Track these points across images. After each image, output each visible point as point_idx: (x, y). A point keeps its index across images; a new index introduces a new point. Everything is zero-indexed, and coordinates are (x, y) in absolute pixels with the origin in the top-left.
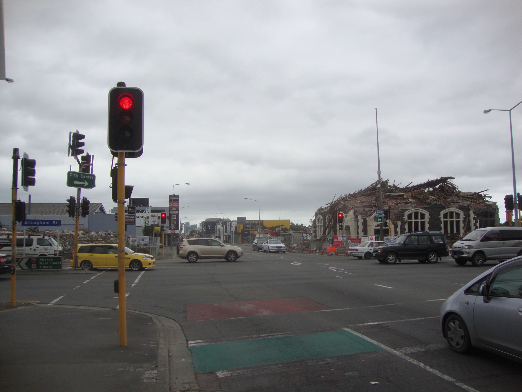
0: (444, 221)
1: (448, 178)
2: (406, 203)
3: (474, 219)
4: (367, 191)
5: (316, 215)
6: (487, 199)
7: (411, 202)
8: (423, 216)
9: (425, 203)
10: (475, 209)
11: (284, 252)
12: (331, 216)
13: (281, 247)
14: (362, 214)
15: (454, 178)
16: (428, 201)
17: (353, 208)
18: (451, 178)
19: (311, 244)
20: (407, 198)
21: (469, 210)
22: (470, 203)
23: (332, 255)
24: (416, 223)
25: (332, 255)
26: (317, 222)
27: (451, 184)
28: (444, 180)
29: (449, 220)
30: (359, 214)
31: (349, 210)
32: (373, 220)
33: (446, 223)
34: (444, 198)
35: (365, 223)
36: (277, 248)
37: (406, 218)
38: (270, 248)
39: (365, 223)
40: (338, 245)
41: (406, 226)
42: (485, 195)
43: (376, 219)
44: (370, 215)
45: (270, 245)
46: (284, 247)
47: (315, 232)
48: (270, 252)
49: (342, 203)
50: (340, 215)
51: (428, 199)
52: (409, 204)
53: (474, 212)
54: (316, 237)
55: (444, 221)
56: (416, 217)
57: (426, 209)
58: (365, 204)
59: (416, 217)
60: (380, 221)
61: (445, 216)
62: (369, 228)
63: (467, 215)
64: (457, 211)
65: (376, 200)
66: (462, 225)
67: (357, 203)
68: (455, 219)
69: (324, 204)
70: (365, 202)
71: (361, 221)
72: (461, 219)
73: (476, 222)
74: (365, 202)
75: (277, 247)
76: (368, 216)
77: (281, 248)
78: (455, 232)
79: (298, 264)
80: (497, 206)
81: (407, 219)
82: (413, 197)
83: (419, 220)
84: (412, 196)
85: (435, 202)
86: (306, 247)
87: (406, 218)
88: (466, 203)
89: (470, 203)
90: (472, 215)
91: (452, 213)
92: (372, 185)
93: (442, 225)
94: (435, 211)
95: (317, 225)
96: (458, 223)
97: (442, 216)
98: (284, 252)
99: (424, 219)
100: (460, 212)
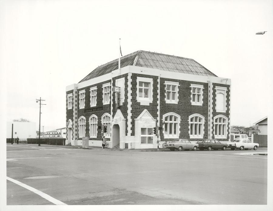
56: (171, 120)
61: (192, 120)
93: (189, 127)
97: (189, 120)
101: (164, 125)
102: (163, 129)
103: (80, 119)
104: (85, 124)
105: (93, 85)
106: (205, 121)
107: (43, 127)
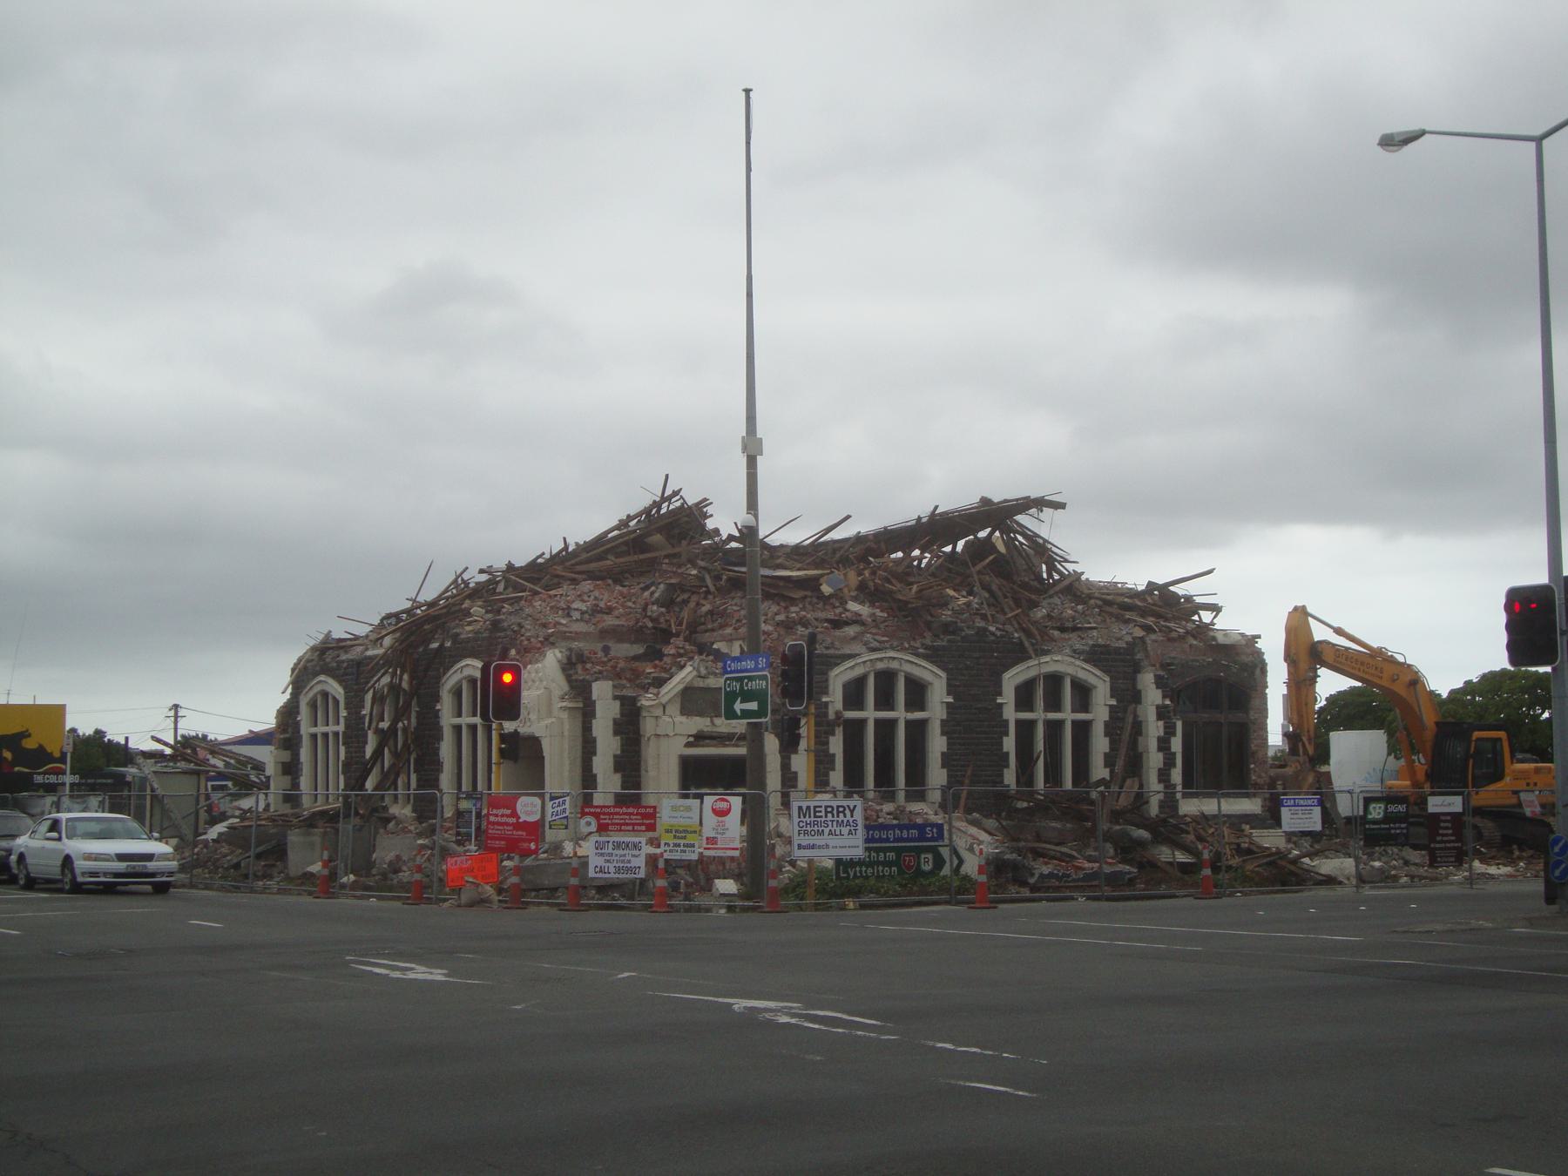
0: (1019, 723)
1: (1026, 505)
2: (837, 624)
3: (1162, 713)
4: (600, 558)
5: (302, 676)
6: (1206, 616)
7: (857, 620)
8: (917, 693)
9: (928, 625)
10: (1164, 666)
11: (161, 889)
12: (411, 682)
13: (149, 857)
14: (616, 675)
15: (1062, 506)
16: (946, 615)
17: (548, 642)
18: (1040, 503)
19: (294, 838)
20: (839, 598)
21: (1137, 669)
22: (1139, 633)
23: (481, 902)
24: (885, 729)
25: (481, 902)
26: (304, 716)
27: (1032, 538)
28: (998, 514)
29: (1039, 715)
30: (600, 676)
31: (532, 652)
32: (674, 709)
33: (1026, 728)
34: (1018, 604)
35: (629, 725)
36: (122, 866)
37: (835, 698)
38: (80, 865)
39: (629, 725)
40: (512, 847)
41: (836, 745)
42: (1189, 599)
43: (691, 700)
44: (659, 683)
45: (78, 847)
46: (164, 857)
47: (290, 769)
48: (78, 888)
49: (477, 610)
50: (507, 678)
51: (945, 605)
52: (851, 631)
53: (1160, 682)
54: (292, 799)
55: (1019, 723)
56: (885, 701)
57: (934, 656)
58: (610, 621)
59: (885, 701)
60: (746, 714)
61: (1025, 696)
62: (650, 752)
63: (1127, 696)
64: (1082, 675)
65: (668, 603)
66: (1100, 744)
67: (567, 612)
68: (1067, 715)
69: (358, 612)
70: (609, 611)
71: (607, 710)
72: (1100, 714)
73: (1170, 731)
74: (609, 611)
75: (122, 857)
76: (645, 688)
77: (152, 866)
78: (1068, 784)
79: (438, 975)
80: (1259, 654)
81: (839, 705)
82: (866, 593)
83: (900, 714)
84: (862, 587)
85: (980, 623)
86: (259, 856)
87: (835, 698)
88: (1123, 634)
89: (1139, 633)
90: (1153, 697)
91: (1054, 681)
92: (623, 524)
93: (1009, 744)
94: (975, 663)
95: (306, 729)
96: (917, 731)
97: (1008, 698)
98: (161, 889)
99: (922, 708)
100: (1092, 680)
101: (839, 732)
102: (833, 762)
103: (311, 694)
104: (341, 728)
105: (1554, 442)
106: (1114, 702)
107: (748, 91)
